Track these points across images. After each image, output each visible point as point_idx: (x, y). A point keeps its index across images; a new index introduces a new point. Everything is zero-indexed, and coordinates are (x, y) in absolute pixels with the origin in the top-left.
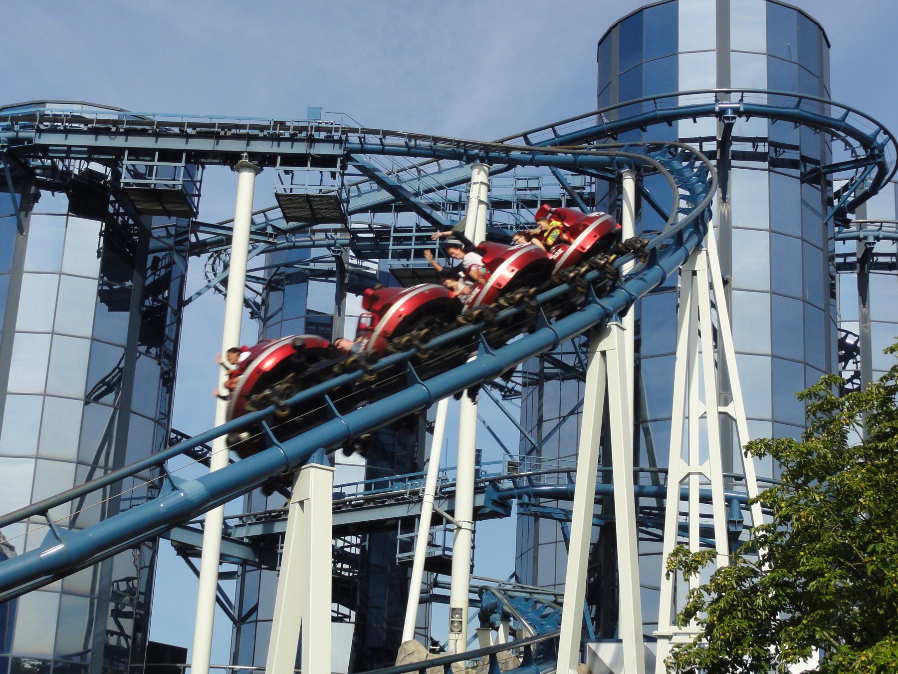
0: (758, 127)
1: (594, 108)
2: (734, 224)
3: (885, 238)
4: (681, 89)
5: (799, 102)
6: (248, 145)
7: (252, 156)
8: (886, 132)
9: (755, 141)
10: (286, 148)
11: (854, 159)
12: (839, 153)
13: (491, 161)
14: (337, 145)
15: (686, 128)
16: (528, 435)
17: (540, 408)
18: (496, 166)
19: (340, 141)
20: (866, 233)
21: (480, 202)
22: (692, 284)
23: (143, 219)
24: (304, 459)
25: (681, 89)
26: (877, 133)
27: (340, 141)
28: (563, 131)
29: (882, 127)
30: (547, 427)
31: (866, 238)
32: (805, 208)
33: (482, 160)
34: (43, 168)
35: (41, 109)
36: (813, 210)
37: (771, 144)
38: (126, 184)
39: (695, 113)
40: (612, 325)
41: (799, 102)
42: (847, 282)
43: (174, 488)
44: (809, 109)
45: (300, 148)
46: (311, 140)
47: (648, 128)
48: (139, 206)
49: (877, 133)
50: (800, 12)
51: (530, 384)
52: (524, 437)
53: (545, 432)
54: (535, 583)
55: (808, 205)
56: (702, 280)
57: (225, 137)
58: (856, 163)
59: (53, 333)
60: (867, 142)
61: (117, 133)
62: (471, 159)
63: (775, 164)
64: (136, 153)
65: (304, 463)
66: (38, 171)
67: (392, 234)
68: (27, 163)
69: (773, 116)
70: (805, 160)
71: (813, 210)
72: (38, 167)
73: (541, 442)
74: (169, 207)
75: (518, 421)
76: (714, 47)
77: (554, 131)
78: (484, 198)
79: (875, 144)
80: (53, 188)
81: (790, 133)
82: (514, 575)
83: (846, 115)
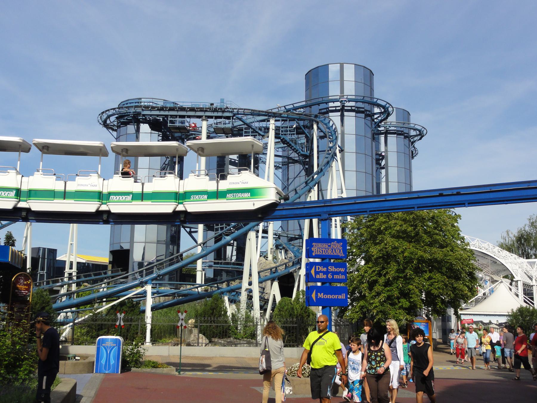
0: (353, 104)
1: (304, 100)
2: (345, 133)
3: (392, 127)
4: (330, 95)
5: (364, 98)
6: (205, 113)
7: (206, 116)
8: (389, 104)
9: (351, 107)
10: (216, 114)
11: (380, 111)
12: (376, 110)
13: (275, 117)
14: (231, 113)
15: (331, 104)
16: (284, 183)
17: (288, 174)
18: (277, 119)
19: (232, 112)
20: (386, 125)
21: (273, 129)
22: (332, 170)
23: (173, 134)
24: (249, 230)
25: (330, 95)
26: (386, 104)
27: (232, 112)
28: (295, 105)
29: (387, 103)
30: (290, 181)
31: (386, 127)
32: (366, 125)
33: (273, 117)
34: (142, 119)
35: (140, 101)
36: (368, 126)
37: (356, 107)
38: (169, 126)
39: (334, 101)
40: (312, 190)
41: (364, 98)
42: (382, 138)
43: (225, 238)
44: (368, 99)
45: (220, 114)
46: (223, 112)
47: (320, 105)
48: (172, 131)
49: (386, 104)
50: (364, 67)
51: (285, 165)
52: (283, 183)
53: (290, 182)
54: (288, 231)
55: (366, 124)
56: (334, 169)
57: (198, 111)
58: (381, 113)
59: (149, 169)
60: (384, 107)
61: (166, 110)
62: (269, 116)
63: (357, 112)
64: (172, 116)
65: (250, 231)
66: (141, 120)
67: (244, 130)
68: (138, 118)
69: (356, 101)
70: (367, 111)
71: (368, 126)
72: (141, 119)
73: (288, 185)
74: (181, 131)
75: (281, 179)
76: (339, 79)
77: (293, 106)
78: (274, 128)
79: (386, 108)
80: (144, 123)
81: (360, 105)
82: (281, 226)
83: (377, 100)
